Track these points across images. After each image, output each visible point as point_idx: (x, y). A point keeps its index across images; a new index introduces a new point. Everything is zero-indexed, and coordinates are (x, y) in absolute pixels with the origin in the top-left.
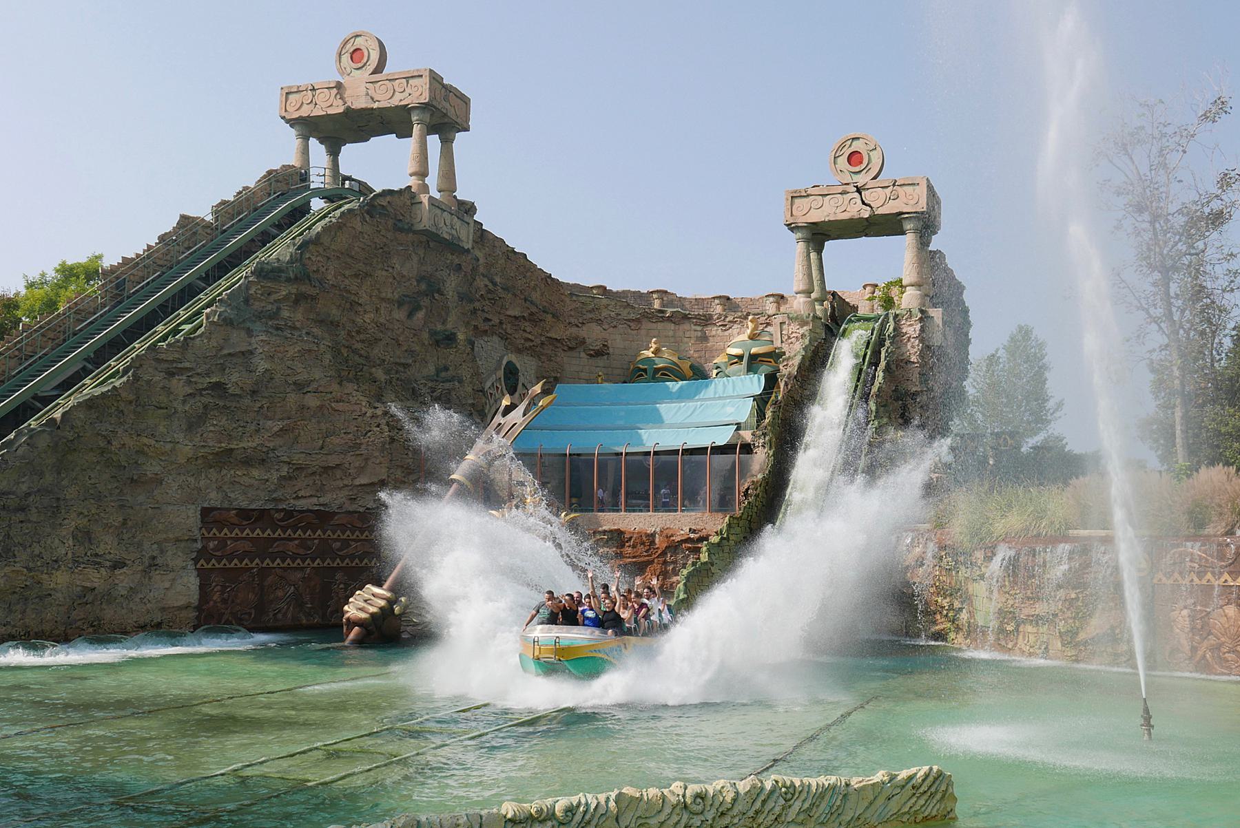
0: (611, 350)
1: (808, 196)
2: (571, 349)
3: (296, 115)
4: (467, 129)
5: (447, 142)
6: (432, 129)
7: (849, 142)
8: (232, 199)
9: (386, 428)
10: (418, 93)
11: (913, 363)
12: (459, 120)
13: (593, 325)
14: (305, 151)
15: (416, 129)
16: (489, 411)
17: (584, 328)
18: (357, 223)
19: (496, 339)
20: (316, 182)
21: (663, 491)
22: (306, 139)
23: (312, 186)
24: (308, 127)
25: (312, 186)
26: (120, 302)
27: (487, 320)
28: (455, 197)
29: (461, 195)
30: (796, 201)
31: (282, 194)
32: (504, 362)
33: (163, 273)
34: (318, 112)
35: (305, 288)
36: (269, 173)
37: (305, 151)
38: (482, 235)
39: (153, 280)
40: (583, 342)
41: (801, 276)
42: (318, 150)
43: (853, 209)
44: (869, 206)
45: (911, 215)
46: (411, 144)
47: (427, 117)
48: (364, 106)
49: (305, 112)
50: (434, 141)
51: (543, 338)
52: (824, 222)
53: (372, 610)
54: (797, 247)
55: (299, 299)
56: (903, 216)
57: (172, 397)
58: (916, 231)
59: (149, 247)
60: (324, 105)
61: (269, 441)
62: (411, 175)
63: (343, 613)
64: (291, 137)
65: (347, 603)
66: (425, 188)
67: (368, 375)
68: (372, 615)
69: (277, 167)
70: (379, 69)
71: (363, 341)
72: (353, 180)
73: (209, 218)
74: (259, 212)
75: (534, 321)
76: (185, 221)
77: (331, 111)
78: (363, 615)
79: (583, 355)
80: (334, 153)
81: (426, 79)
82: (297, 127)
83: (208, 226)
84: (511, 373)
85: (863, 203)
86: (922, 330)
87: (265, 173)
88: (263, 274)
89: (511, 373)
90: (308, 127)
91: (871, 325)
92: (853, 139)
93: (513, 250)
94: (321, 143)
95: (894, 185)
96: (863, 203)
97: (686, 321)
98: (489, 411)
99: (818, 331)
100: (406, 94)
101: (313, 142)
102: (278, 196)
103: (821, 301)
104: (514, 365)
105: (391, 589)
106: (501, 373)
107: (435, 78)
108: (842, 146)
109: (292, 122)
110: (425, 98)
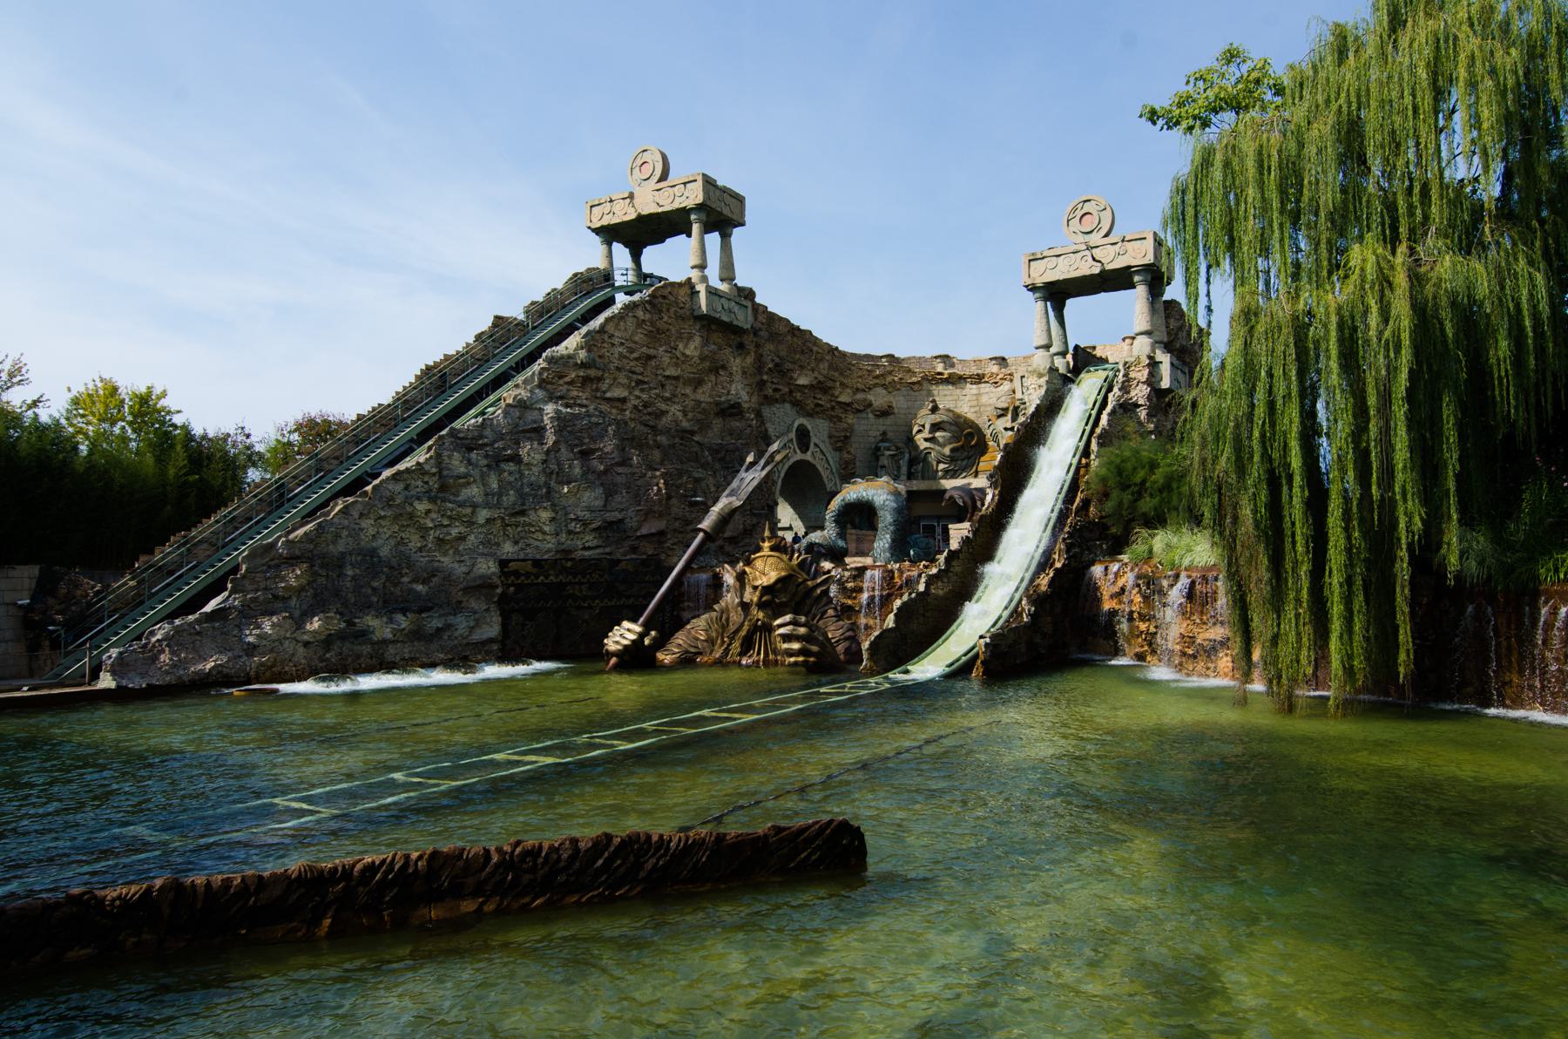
0: (896, 411)
1: (1043, 258)
2: (859, 411)
3: (598, 225)
4: (743, 224)
5: (725, 236)
6: (708, 228)
8: (541, 299)
10: (694, 196)
11: (1141, 405)
12: (734, 217)
13: (880, 390)
15: (696, 228)
16: (1546, 402)
18: (640, 313)
19: (788, 406)
20: (619, 280)
22: (609, 244)
23: (617, 284)
24: (610, 234)
25: (617, 284)
28: (736, 285)
29: (741, 281)
30: (1073, 306)
32: (796, 425)
34: (616, 220)
35: (592, 373)
36: (575, 275)
40: (870, 405)
41: (1039, 332)
42: (621, 254)
43: (1087, 268)
44: (1100, 262)
46: (694, 241)
47: (703, 216)
48: (652, 211)
49: (605, 222)
51: (833, 404)
52: (1058, 281)
53: (626, 642)
54: (1036, 308)
55: (586, 380)
58: (1144, 282)
59: (468, 345)
60: (621, 213)
62: (693, 268)
63: (604, 645)
65: (607, 637)
66: (704, 279)
68: (625, 646)
69: (582, 269)
70: (664, 176)
71: (650, 414)
73: (521, 317)
74: (565, 307)
76: (499, 320)
78: (619, 647)
79: (871, 415)
80: (636, 256)
81: (700, 183)
82: (728, 232)
83: (520, 324)
85: (1094, 259)
86: (1151, 374)
87: (570, 276)
90: (610, 234)
92: (1085, 201)
93: (798, 328)
94: (626, 247)
95: (1123, 241)
96: (1094, 259)
98: (1546, 402)
99: (1055, 381)
100: (684, 198)
103: (1063, 354)
106: (793, 435)
107: (709, 182)
108: (1075, 209)
109: (597, 231)
110: (700, 200)
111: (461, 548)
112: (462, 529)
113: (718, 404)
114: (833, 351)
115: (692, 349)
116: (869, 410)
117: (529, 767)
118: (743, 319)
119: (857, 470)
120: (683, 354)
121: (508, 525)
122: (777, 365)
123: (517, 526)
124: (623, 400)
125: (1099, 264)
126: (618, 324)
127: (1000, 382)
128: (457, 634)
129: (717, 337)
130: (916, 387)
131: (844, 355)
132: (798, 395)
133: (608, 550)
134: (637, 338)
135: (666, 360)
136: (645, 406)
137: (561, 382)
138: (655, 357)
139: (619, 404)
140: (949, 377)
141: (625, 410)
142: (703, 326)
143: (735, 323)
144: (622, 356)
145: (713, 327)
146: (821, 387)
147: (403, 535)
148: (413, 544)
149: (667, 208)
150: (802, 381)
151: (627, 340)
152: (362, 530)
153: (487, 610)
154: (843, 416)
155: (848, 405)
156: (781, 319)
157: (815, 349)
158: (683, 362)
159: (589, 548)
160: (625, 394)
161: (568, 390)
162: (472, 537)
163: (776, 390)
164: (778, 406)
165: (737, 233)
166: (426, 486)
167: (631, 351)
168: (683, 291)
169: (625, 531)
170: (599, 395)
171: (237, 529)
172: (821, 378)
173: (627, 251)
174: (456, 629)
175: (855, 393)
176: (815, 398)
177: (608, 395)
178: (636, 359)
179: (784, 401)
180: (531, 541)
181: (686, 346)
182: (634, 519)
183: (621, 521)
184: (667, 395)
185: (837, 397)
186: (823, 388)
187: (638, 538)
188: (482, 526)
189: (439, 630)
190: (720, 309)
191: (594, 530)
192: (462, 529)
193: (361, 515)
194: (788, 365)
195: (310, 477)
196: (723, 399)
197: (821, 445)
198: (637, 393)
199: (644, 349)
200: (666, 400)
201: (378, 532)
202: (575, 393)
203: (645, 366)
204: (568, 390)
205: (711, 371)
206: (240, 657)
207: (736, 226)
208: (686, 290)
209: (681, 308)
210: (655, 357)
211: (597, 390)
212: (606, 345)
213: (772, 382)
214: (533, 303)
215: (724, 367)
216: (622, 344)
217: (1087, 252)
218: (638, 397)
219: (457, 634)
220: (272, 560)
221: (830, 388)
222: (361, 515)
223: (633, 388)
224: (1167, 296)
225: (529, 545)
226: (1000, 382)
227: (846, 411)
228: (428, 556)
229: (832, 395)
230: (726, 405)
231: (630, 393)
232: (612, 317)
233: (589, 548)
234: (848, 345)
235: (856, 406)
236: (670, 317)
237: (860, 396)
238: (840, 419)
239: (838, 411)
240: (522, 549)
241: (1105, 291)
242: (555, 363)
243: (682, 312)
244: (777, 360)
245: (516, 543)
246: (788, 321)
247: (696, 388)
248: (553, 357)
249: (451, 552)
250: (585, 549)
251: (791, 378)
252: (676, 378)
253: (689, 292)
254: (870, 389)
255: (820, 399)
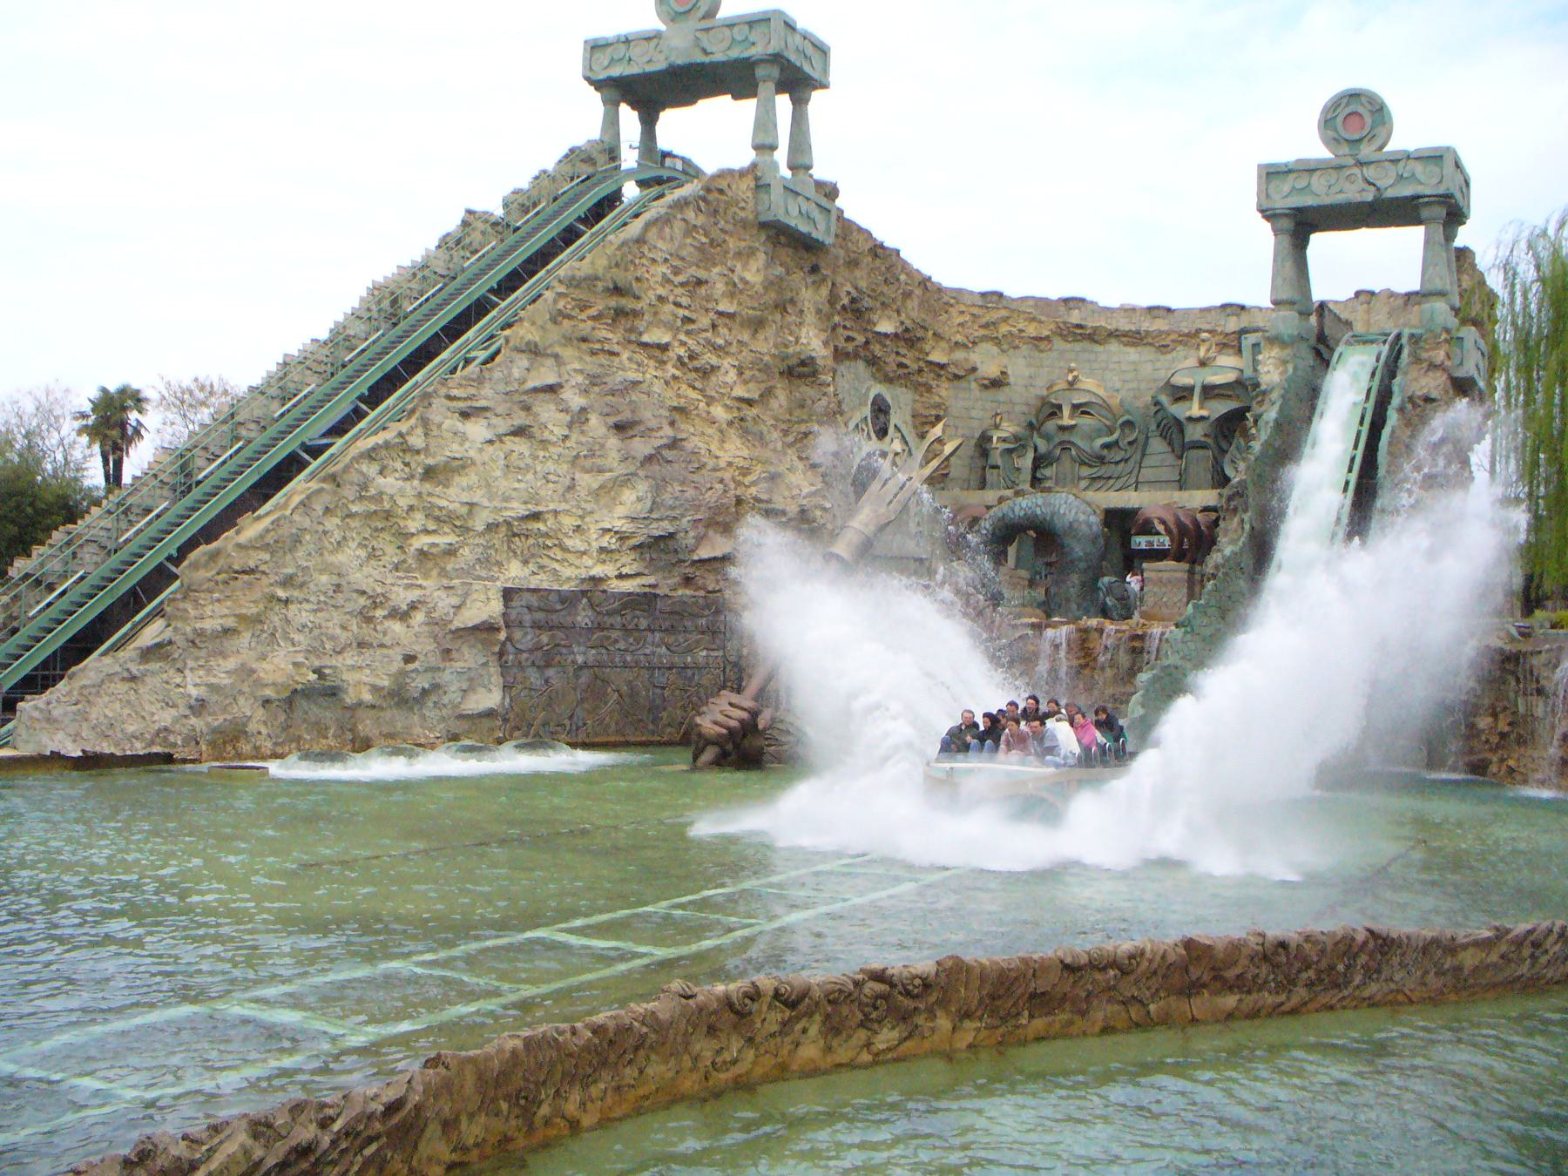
0: (1012, 380)
2: (957, 377)
4: (824, 86)
5: (799, 103)
6: (782, 87)
7: (1345, 100)
9: (732, 485)
12: (816, 75)
14: (611, 122)
17: (976, 349)
18: (690, 214)
19: (861, 365)
20: (629, 159)
21: (1106, 579)
22: (611, 105)
26: (395, 325)
27: (849, 339)
28: (811, 176)
29: (818, 173)
30: (1321, 244)
31: (588, 178)
32: (872, 396)
33: (445, 285)
34: (634, 70)
37: (611, 122)
38: (847, 228)
39: (433, 295)
40: (974, 369)
42: (629, 119)
43: (1353, 192)
45: (1432, 199)
49: (616, 72)
50: (783, 103)
51: (922, 364)
56: (1421, 200)
57: (467, 445)
61: (586, 501)
64: (593, 102)
67: (704, 415)
72: (675, 157)
75: (858, 310)
77: (649, 68)
79: (974, 385)
80: (649, 122)
84: (880, 410)
88: (574, 283)
89: (880, 410)
91: (1374, 349)
93: (882, 246)
94: (633, 108)
97: (1113, 340)
101: (624, 109)
102: (583, 181)
104: (884, 400)
105: (756, 699)
106: (867, 411)
109: (598, 85)
111: (449, 567)
112: (452, 539)
113: (784, 358)
114: (925, 282)
115: (753, 272)
116: (972, 377)
117: (684, 899)
118: (821, 232)
119: (952, 470)
120: (742, 279)
121: (515, 535)
122: (853, 301)
123: (527, 537)
124: (664, 348)
125: (1372, 188)
126: (661, 230)
127: (1172, 345)
128: (446, 700)
129: (785, 254)
130: (1043, 345)
131: (940, 290)
132: (877, 349)
133: (651, 580)
134: (684, 253)
135: (720, 287)
136: (691, 358)
137: (583, 316)
138: (707, 282)
139: (657, 353)
140: (1094, 333)
141: (665, 363)
142: (768, 238)
143: (815, 235)
144: (666, 280)
145: (782, 239)
146: (908, 338)
147: (375, 543)
148: (387, 558)
149: (719, 57)
150: (886, 326)
151: (671, 255)
152: (325, 533)
153: (485, 665)
154: (934, 383)
155: (942, 367)
156: (860, 230)
157: (903, 277)
158: (741, 292)
159: (627, 576)
160: (666, 339)
161: (594, 329)
162: (465, 551)
163: (849, 339)
164: (848, 363)
165: (817, 96)
166: (407, 470)
167: (676, 271)
168: (744, 187)
169: (676, 551)
170: (633, 337)
171: (131, 524)
172: (908, 323)
173: (635, 114)
174: (445, 693)
175: (952, 350)
176: (898, 353)
177: (646, 338)
178: (682, 285)
179: (856, 356)
180: (545, 561)
181: (745, 266)
182: (692, 534)
183: (671, 536)
184: (720, 342)
185: (927, 354)
186: (910, 339)
187: (694, 562)
188: (482, 534)
189: (425, 692)
190: (796, 213)
191: (634, 548)
192: (452, 539)
193: (327, 510)
194: (867, 302)
195: (224, 449)
196: (791, 350)
197: (903, 429)
198: (682, 337)
199: (693, 271)
200: (717, 349)
201: (344, 538)
202: (603, 333)
203: (691, 295)
204: (594, 329)
205: (776, 306)
206: (186, 717)
207: (815, 88)
208: (749, 182)
209: (743, 209)
210: (707, 282)
211: (631, 330)
212: (644, 261)
213: (845, 327)
214: (515, 192)
215: (792, 301)
216: (666, 260)
217: (1356, 171)
218: (683, 344)
219: (446, 700)
220: (218, 574)
221: (919, 339)
222: (327, 510)
223: (678, 329)
224: (1459, 242)
225: (542, 567)
226: (1172, 345)
227: (939, 376)
228: (407, 578)
229: (921, 350)
230: (794, 361)
231: (674, 337)
232: (657, 219)
233: (627, 576)
234: (946, 275)
235: (952, 369)
236: (726, 222)
237: (959, 355)
238: (929, 389)
239: (928, 377)
240: (534, 573)
241: (1368, 226)
242: (577, 286)
243: (742, 214)
244: (855, 294)
245: (525, 562)
246: (870, 234)
247: (756, 331)
248: (573, 278)
249: (435, 573)
250: (620, 577)
251: (869, 321)
252: (731, 316)
253: (752, 185)
254: (974, 343)
255: (904, 356)
